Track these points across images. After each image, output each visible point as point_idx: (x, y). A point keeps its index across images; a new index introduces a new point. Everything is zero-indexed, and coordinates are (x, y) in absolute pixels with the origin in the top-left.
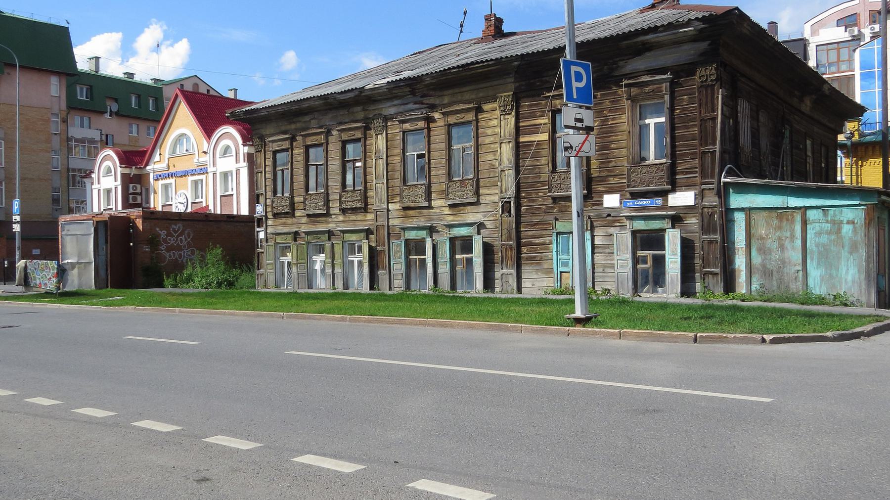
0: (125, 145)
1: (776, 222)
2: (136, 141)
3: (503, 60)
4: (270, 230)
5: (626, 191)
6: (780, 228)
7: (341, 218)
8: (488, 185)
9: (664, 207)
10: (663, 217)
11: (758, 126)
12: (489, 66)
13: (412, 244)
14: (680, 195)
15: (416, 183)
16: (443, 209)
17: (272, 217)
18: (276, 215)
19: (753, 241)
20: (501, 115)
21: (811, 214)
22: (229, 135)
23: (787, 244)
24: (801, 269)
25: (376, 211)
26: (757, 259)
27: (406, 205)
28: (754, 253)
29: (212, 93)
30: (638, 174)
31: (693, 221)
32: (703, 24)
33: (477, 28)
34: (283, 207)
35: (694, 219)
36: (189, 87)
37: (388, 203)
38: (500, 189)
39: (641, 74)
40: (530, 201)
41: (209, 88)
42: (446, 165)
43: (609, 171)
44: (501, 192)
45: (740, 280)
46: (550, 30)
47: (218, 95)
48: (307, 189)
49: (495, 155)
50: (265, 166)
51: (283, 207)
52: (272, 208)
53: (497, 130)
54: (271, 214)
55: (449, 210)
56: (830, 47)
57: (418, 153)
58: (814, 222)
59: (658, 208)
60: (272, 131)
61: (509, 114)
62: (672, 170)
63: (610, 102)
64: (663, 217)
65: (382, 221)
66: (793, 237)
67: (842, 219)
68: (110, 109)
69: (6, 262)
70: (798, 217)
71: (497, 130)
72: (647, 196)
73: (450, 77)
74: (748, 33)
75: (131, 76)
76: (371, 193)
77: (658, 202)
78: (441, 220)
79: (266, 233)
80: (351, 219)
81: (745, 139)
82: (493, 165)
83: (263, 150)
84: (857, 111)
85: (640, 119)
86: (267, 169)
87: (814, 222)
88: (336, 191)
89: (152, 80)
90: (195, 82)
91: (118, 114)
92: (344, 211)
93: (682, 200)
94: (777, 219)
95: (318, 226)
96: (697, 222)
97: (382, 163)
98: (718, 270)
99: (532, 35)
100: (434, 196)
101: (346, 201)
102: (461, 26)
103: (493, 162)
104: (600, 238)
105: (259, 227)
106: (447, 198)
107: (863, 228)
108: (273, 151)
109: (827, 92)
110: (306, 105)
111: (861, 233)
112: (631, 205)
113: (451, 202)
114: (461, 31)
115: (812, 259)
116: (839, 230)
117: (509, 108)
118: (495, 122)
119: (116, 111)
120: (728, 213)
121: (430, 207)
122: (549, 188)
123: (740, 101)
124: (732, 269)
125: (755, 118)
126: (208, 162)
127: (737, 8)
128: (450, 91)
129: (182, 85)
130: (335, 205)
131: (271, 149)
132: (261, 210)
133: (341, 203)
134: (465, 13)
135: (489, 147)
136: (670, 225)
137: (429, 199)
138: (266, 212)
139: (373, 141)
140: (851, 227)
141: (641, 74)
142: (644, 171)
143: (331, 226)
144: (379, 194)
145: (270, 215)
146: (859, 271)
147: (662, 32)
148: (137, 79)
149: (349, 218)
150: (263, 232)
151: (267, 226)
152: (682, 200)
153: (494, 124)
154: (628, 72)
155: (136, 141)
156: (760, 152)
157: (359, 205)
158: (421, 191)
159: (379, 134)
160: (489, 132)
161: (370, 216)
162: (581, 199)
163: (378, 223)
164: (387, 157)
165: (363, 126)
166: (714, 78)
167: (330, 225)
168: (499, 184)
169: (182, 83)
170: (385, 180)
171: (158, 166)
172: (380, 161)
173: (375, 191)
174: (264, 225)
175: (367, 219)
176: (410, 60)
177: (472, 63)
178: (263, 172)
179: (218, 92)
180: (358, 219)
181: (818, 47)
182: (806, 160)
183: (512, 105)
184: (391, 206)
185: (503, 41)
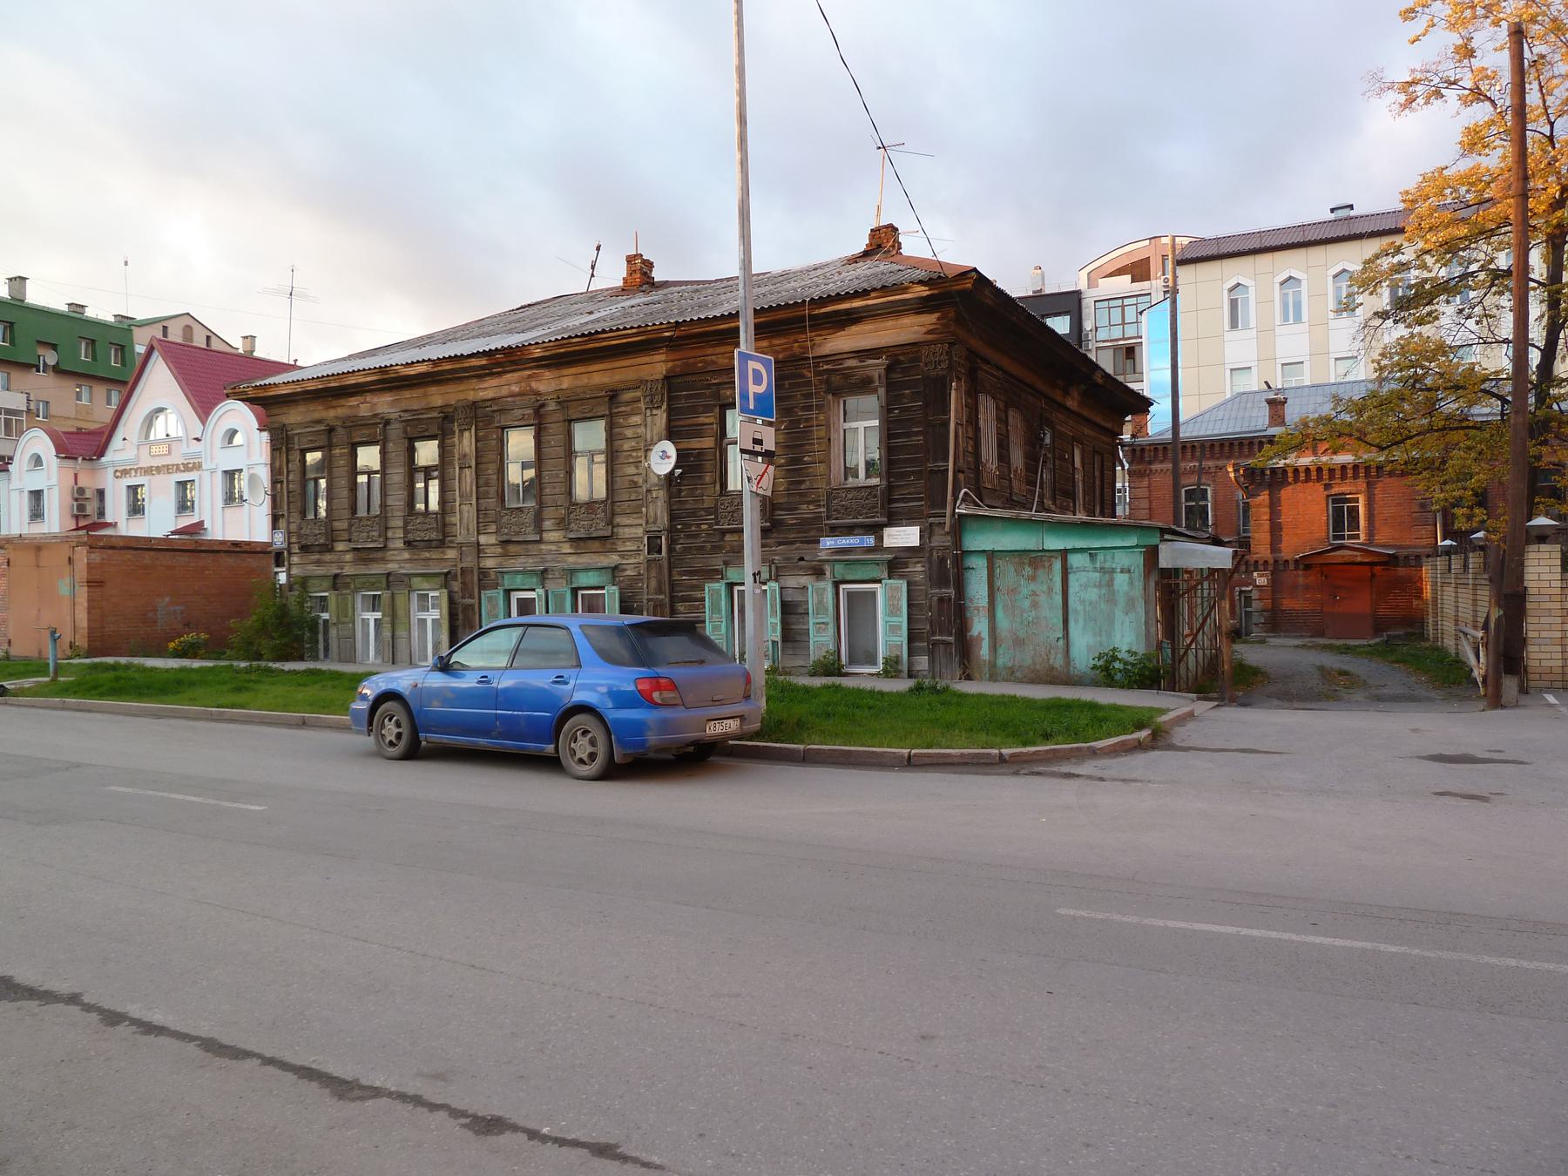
0: (69, 418)
1: (1028, 570)
2: (88, 413)
4: (294, 571)
5: (825, 525)
6: (1033, 578)
7: (406, 555)
8: (628, 511)
9: (879, 547)
10: (877, 563)
11: (1007, 430)
13: (715, 355)
15: (521, 505)
16: (561, 545)
17: (297, 551)
18: (305, 549)
19: (1071, 577)
20: (646, 409)
21: (1075, 560)
22: (237, 415)
23: (1043, 599)
24: (1061, 636)
25: (460, 546)
27: (505, 538)
29: (215, 345)
30: (841, 501)
31: (918, 569)
32: (929, 290)
33: (613, 274)
34: (316, 535)
36: (176, 336)
37: (478, 534)
38: (644, 518)
39: (845, 356)
40: (688, 537)
41: (210, 334)
42: (566, 480)
43: (801, 495)
44: (647, 522)
45: (981, 652)
46: (721, 280)
47: (228, 349)
48: (354, 509)
49: (637, 468)
50: (288, 472)
51: (316, 535)
52: (299, 536)
53: (641, 430)
54: (296, 546)
55: (571, 547)
56: (1112, 303)
58: (1079, 570)
59: (869, 550)
60: (299, 418)
61: (658, 408)
62: (889, 495)
63: (803, 395)
65: (469, 562)
66: (1050, 590)
67: (1114, 566)
68: (44, 360)
70: (1057, 565)
71: (641, 430)
72: (855, 532)
74: (990, 302)
75: (79, 310)
76: (452, 519)
77: (870, 541)
78: (558, 562)
79: (289, 576)
80: (422, 557)
81: (989, 452)
82: (635, 483)
83: (284, 448)
84: (1142, 405)
85: (845, 421)
86: (290, 478)
87: (1079, 570)
88: (399, 514)
89: (115, 316)
90: (189, 324)
91: (58, 370)
92: (409, 544)
94: (1029, 566)
95: (370, 567)
96: (923, 569)
97: (469, 475)
98: (951, 639)
99: (695, 287)
100: (547, 524)
102: (593, 267)
103: (635, 479)
105: (278, 566)
106: (567, 529)
107: (1142, 579)
109: (1100, 381)
110: (352, 381)
111: (1139, 584)
113: (572, 535)
114: (593, 275)
115: (1076, 621)
116: (1111, 583)
117: (657, 398)
118: (636, 419)
119: (53, 364)
121: (540, 541)
122: (716, 518)
123: (982, 397)
124: (971, 636)
125: (1002, 420)
126: (203, 454)
127: (975, 270)
129: (165, 328)
130: (398, 536)
131: (296, 447)
133: (406, 532)
134: (598, 248)
135: (631, 455)
136: (885, 574)
137: (540, 531)
138: (289, 543)
139: (456, 440)
140: (1126, 577)
141: (845, 356)
142: (850, 496)
143: (392, 567)
144: (465, 521)
145: (295, 549)
146: (1137, 637)
148: (90, 313)
150: (285, 574)
151: (290, 564)
154: (828, 352)
155: (88, 413)
156: (1009, 468)
157: (434, 536)
158: (528, 518)
159: (465, 429)
161: (451, 554)
162: (758, 533)
163: (464, 565)
164: (477, 464)
165: (441, 417)
166: (944, 366)
167: (389, 566)
168: (644, 509)
169: (165, 324)
170: (475, 500)
171: (119, 457)
172: (467, 471)
173: (458, 516)
174: (286, 563)
176: (515, 317)
177: (604, 331)
178: (285, 482)
180: (433, 557)
181: (1097, 304)
182: (1073, 474)
183: (663, 395)
184: (483, 539)
185: (656, 296)
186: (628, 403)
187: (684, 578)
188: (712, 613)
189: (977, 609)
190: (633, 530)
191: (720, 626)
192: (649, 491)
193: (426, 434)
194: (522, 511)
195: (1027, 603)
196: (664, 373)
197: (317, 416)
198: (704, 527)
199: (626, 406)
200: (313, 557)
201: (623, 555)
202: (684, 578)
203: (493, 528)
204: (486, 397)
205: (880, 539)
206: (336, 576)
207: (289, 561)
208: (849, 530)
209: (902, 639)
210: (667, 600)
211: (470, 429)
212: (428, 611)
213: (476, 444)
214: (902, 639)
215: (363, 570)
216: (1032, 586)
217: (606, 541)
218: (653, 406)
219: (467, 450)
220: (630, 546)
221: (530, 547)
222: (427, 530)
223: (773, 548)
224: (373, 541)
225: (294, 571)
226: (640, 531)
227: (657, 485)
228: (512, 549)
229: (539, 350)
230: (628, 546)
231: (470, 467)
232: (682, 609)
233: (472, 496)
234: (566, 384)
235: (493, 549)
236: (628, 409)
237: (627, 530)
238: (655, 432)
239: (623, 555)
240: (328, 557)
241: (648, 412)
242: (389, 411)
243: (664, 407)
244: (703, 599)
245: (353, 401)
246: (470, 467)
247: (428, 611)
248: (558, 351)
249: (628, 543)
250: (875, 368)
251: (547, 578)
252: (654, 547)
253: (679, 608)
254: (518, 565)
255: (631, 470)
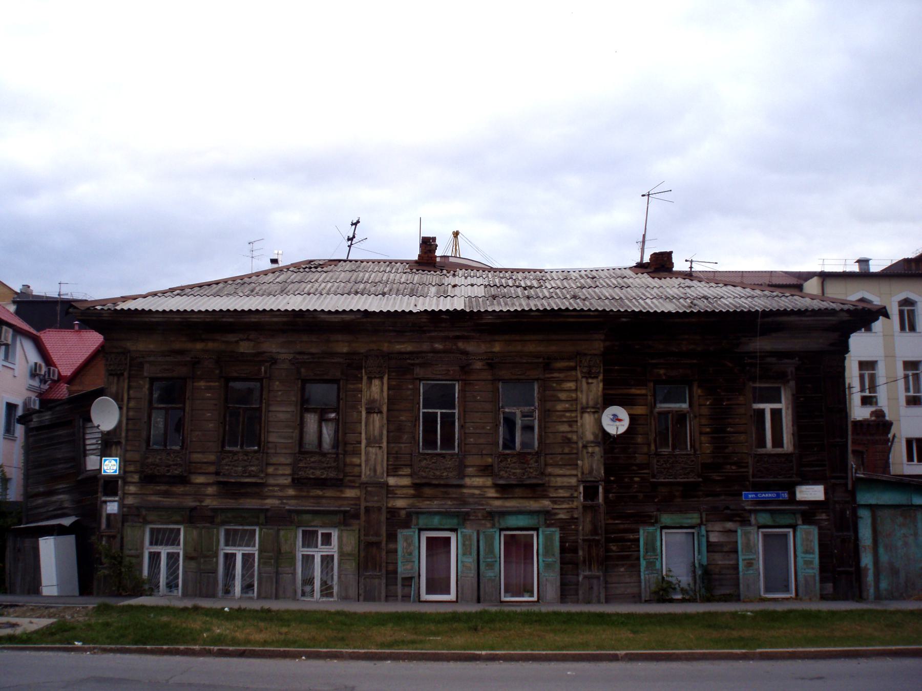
3: (533, 314)
7: (291, 492)
9: (792, 499)
10: (793, 512)
12: (589, 316)
14: (807, 489)
16: (486, 490)
26: (884, 557)
28: (881, 550)
35: (824, 515)
37: (388, 475)
45: (868, 579)
49: (570, 426)
55: (497, 492)
57: (444, 411)
59: (784, 502)
64: (793, 512)
69: (569, 673)
73: (525, 320)
77: (785, 495)
78: (482, 505)
92: (298, 482)
93: (811, 494)
96: (828, 518)
101: (306, 467)
103: (569, 436)
104: (716, 534)
105: (106, 495)
108: (149, 378)
110: (254, 319)
112: (753, 498)
113: (501, 482)
120: (855, 507)
128: (507, 337)
132: (115, 468)
147: (807, 316)
149: (308, 492)
151: (124, 494)
152: (811, 494)
153: (570, 387)
160: (563, 396)
172: (376, 417)
174: (120, 493)
175: (344, 496)
179: (483, 264)
186: (560, 370)
187: (617, 522)
188: (647, 552)
189: (864, 547)
190: (566, 479)
191: (655, 562)
192: (585, 447)
193: (326, 377)
194: (444, 457)
195: (900, 543)
196: (602, 349)
197: (177, 346)
198: (637, 479)
199: (559, 373)
200: (158, 488)
201: (554, 501)
202: (617, 522)
203: (408, 471)
204: (403, 350)
205: (793, 494)
206: (193, 509)
207: (123, 490)
208: (767, 487)
209: (815, 571)
210: (603, 540)
211: (381, 378)
212: (317, 547)
213: (388, 392)
214: (815, 571)
215: (230, 503)
216: (903, 531)
217: (536, 490)
218: (589, 375)
219: (377, 396)
220: (562, 493)
221: (450, 490)
222: (324, 468)
223: (702, 499)
224: (250, 476)
225: (130, 501)
226: (573, 481)
227: (592, 442)
228: (428, 491)
229: (490, 317)
230: (560, 493)
231: (380, 412)
232: (614, 548)
233: (381, 438)
234: (497, 348)
235: (405, 491)
236: (562, 375)
237: (559, 479)
238: (591, 397)
239: (554, 501)
240: (179, 489)
241: (584, 380)
242: (279, 350)
243: (601, 377)
244: (638, 540)
245: (232, 338)
246: (380, 412)
247: (317, 547)
248: (511, 320)
249: (560, 491)
250: (790, 366)
251: (468, 520)
252: (590, 492)
253: (612, 547)
254: (434, 507)
255: (565, 428)
